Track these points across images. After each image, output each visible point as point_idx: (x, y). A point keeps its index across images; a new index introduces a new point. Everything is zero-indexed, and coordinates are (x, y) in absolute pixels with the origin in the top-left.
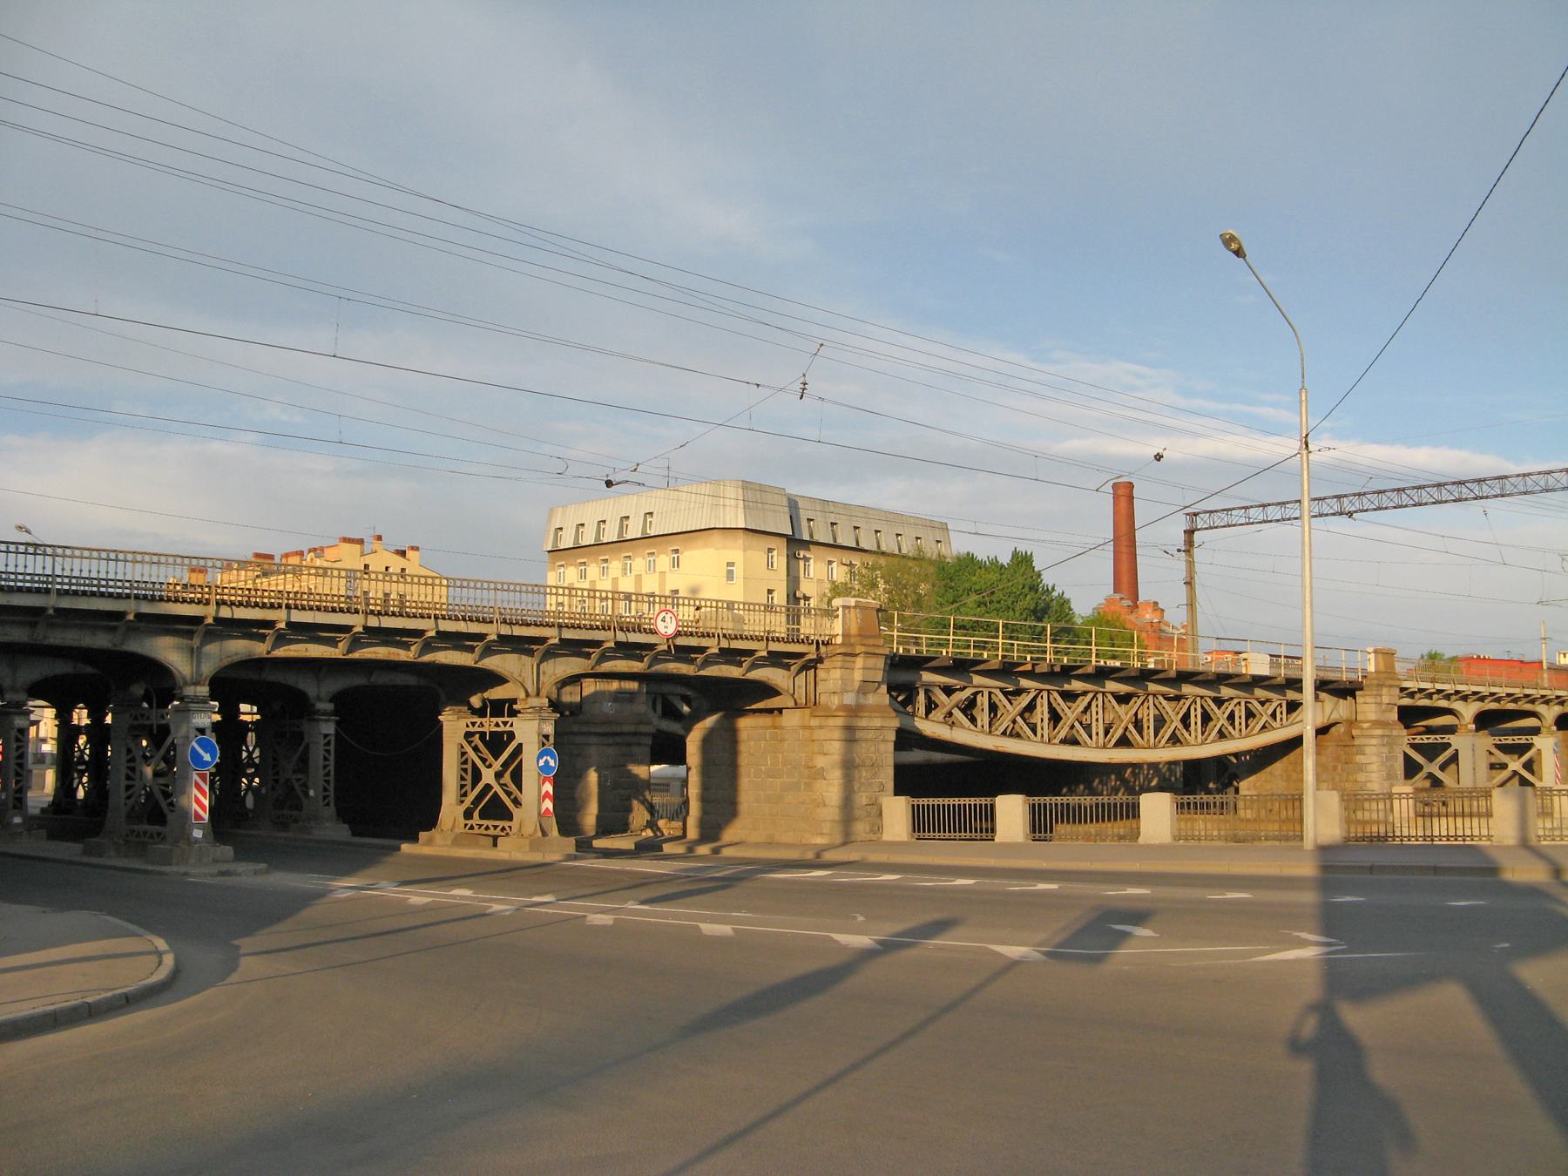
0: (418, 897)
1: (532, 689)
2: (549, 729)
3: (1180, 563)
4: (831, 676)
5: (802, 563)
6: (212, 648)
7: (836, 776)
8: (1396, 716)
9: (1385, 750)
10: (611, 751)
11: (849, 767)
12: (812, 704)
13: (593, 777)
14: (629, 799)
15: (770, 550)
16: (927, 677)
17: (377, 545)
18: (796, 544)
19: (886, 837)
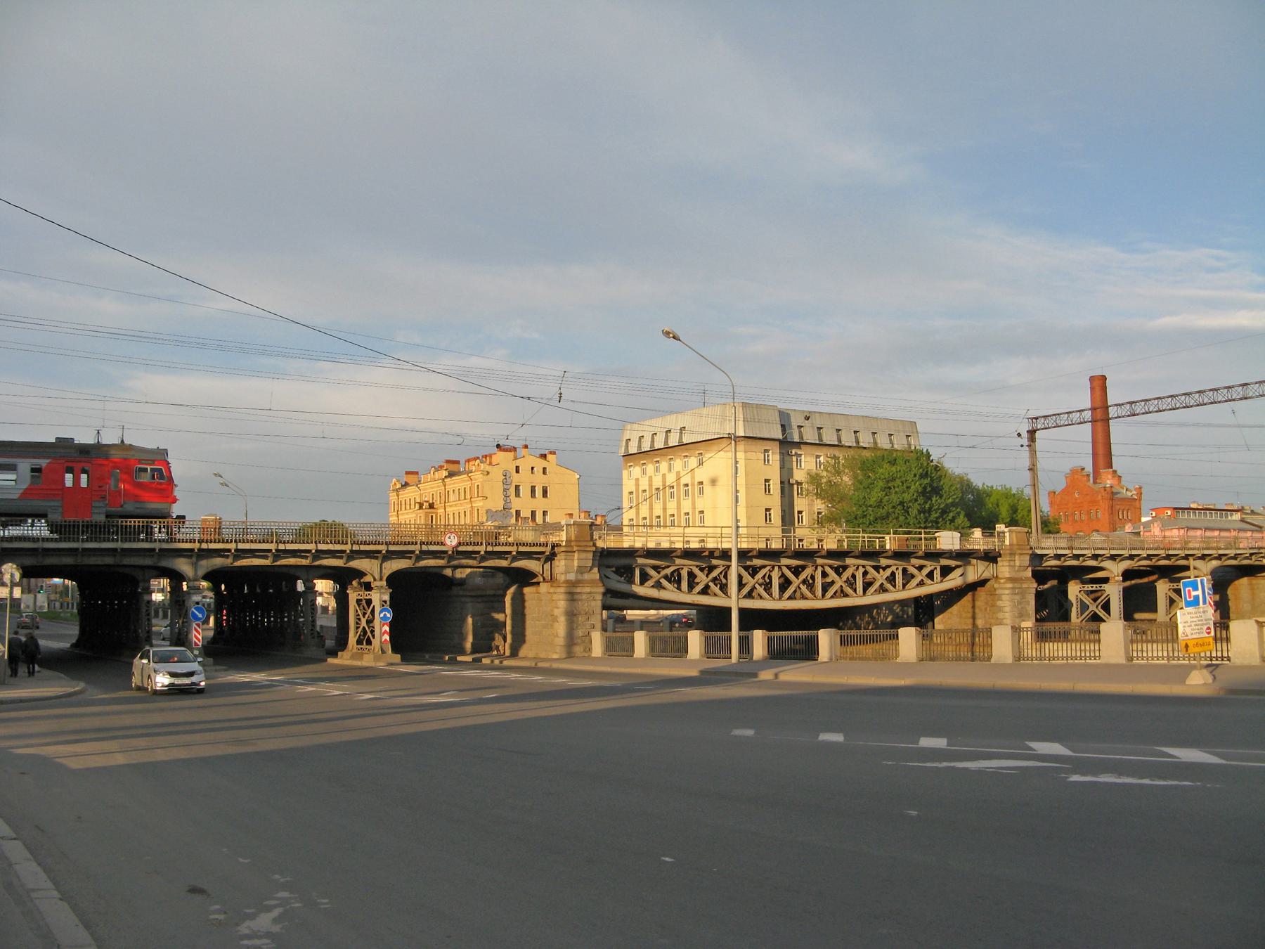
0: (335, 690)
1: (377, 577)
2: (387, 597)
3: (1025, 453)
4: (560, 564)
5: (794, 459)
6: (204, 562)
7: (562, 619)
8: (1030, 574)
9: (1017, 597)
10: (481, 606)
11: (571, 615)
12: (552, 579)
13: (470, 620)
14: (492, 632)
15: (766, 451)
16: (640, 561)
17: (524, 452)
18: (787, 445)
19: (593, 655)
